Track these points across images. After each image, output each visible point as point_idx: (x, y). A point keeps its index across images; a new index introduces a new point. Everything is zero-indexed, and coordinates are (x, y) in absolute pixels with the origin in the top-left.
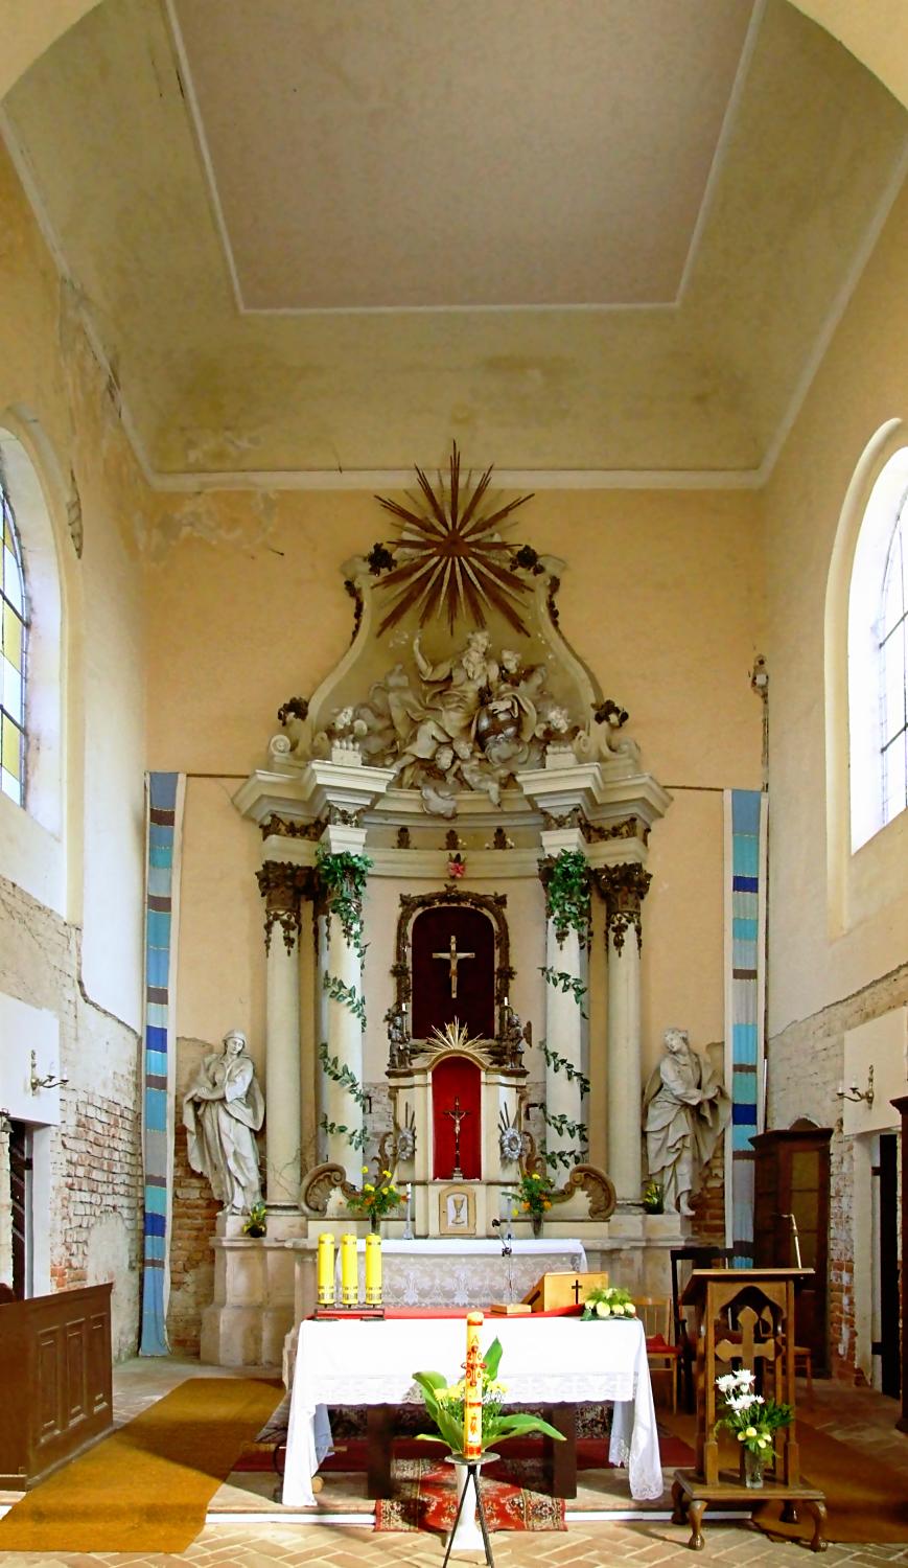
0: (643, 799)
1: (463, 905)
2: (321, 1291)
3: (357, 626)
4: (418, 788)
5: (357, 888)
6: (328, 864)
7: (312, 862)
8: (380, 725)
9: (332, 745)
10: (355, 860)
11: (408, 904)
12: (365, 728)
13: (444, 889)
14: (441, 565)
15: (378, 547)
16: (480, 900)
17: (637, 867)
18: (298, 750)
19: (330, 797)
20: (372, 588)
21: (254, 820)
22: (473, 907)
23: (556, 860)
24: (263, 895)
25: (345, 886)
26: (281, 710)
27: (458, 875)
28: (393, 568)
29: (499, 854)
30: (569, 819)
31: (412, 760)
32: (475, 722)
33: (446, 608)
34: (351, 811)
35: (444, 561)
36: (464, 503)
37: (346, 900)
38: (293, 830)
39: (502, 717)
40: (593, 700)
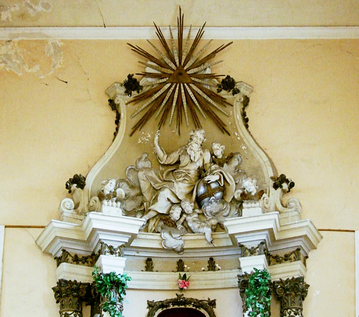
0: (306, 236)
1: (188, 306)
2: (225, 165)
3: (117, 129)
4: (158, 232)
5: (120, 296)
6: (102, 280)
7: (90, 280)
8: (133, 193)
9: (102, 204)
10: (119, 277)
11: (153, 307)
12: (124, 194)
13: (176, 297)
14: (172, 88)
15: (130, 77)
16: (199, 304)
17: (301, 280)
18: (80, 209)
19: (101, 237)
20: (127, 104)
21: (51, 255)
22: (194, 308)
23: (249, 275)
24: (57, 302)
25: (112, 293)
26: (67, 182)
27: (185, 288)
28: (140, 91)
29: (211, 274)
30: (258, 249)
31: (154, 214)
32: (195, 188)
33: (175, 117)
34: (115, 247)
35: (174, 86)
36: (186, 50)
37: (114, 303)
38: (76, 260)
39: (213, 186)
40: (271, 174)
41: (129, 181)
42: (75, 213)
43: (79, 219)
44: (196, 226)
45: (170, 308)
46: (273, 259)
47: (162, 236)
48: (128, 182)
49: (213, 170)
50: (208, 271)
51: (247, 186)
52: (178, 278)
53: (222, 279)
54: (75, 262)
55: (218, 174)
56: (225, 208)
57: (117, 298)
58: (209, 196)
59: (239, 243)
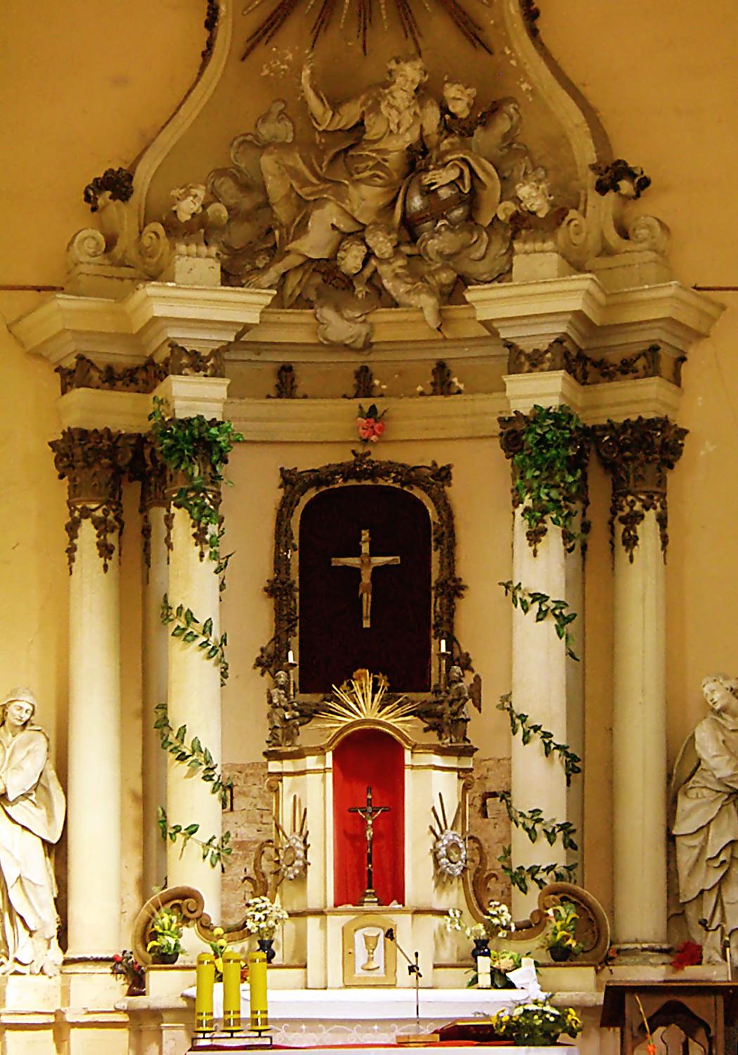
1: (381, 482)
3: (210, 45)
7: (144, 427)
16: (409, 475)
18: (117, 251)
19: (174, 333)
22: (397, 486)
26: (88, 187)
27: (374, 438)
29: (439, 403)
30: (549, 355)
31: (300, 260)
32: (401, 194)
41: (238, 175)
42: (107, 262)
43: (117, 278)
44: (403, 289)
45: (337, 486)
46: (592, 367)
47: (318, 316)
48: (234, 175)
49: (447, 152)
50: (432, 395)
51: (527, 197)
52: (357, 414)
53: (465, 416)
54: (107, 384)
55: (456, 165)
56: (476, 241)
57: (207, 475)
58: (433, 219)
59: (504, 339)
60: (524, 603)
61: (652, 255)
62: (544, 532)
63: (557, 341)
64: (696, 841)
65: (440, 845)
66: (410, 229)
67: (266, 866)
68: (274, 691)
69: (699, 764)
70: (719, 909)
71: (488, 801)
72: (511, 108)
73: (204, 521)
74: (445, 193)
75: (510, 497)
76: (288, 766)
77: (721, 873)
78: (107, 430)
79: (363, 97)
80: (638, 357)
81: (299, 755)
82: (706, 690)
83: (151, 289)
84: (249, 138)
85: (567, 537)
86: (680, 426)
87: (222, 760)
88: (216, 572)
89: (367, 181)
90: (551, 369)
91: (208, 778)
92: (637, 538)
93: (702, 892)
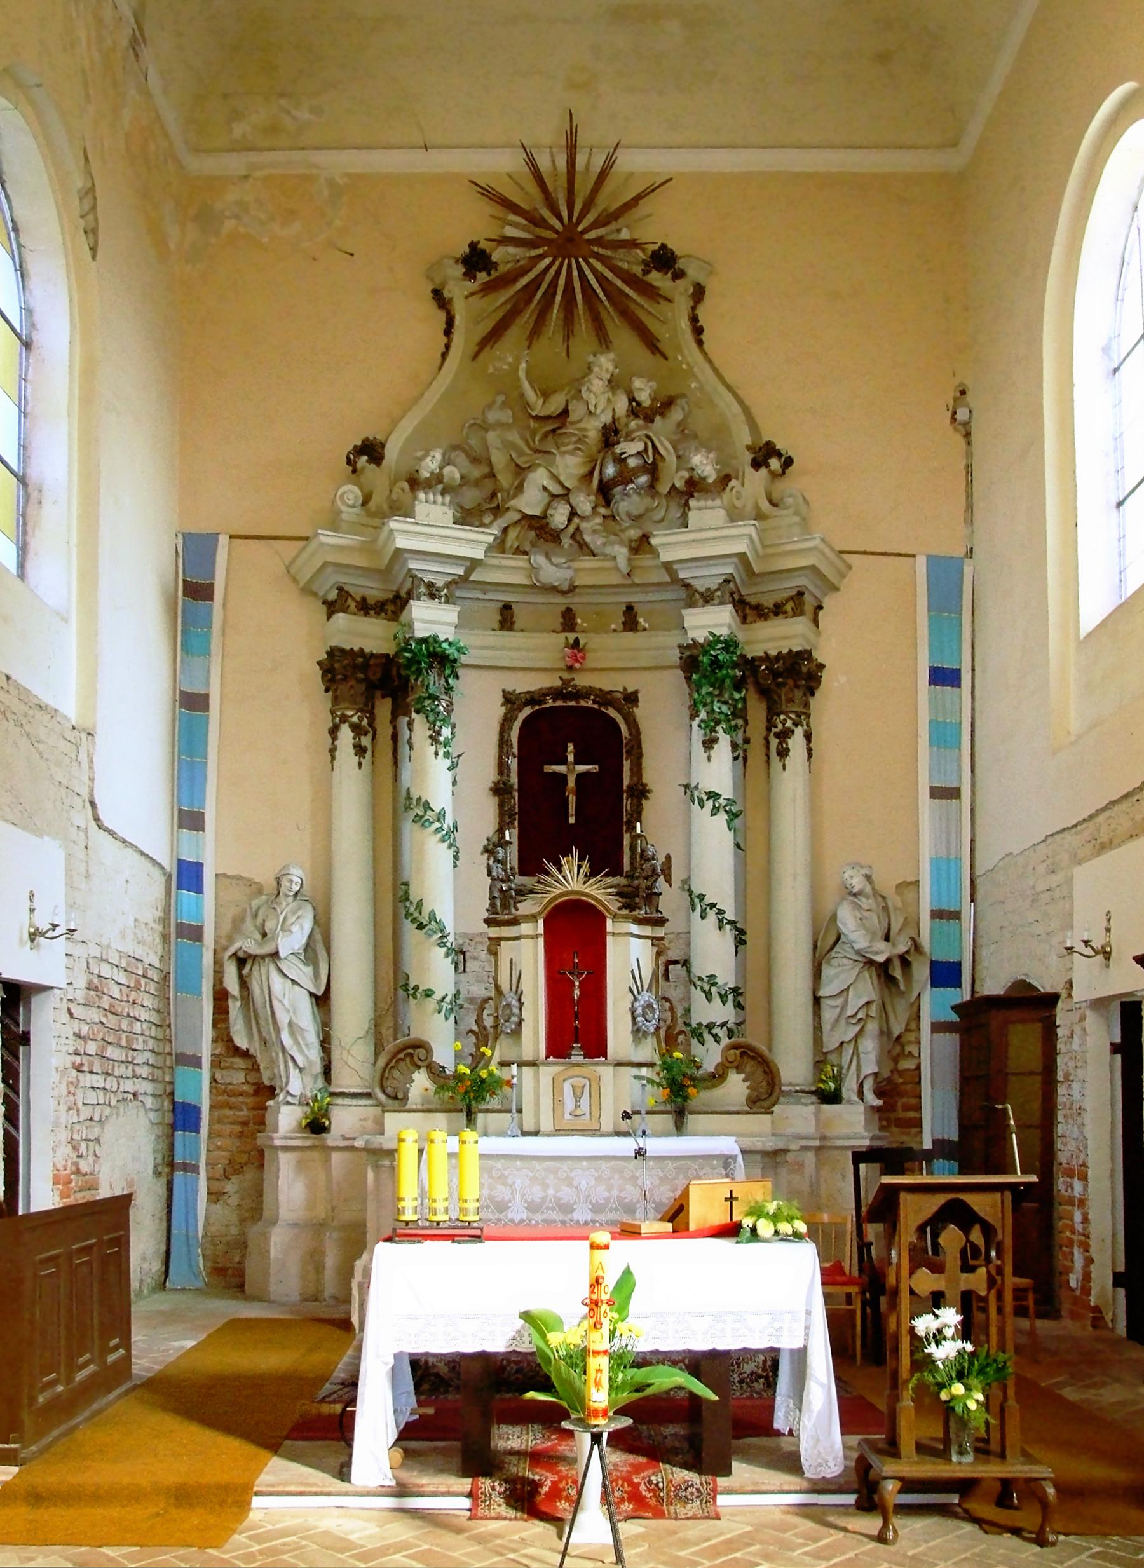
1: (583, 703)
7: (389, 648)
16: (605, 698)
18: (372, 505)
19: (413, 565)
22: (596, 706)
27: (577, 665)
30: (719, 593)
31: (517, 516)
60: (701, 801)
61: (796, 519)
62: (715, 741)
63: (725, 581)
64: (839, 1001)
65: (637, 1004)
66: (605, 492)
67: (488, 1022)
68: (494, 866)
69: (839, 938)
70: (855, 1058)
71: (670, 967)
72: (681, 402)
73: (438, 724)
74: (633, 462)
75: (686, 713)
76: (506, 932)
77: (857, 1028)
78: (361, 650)
79: (567, 389)
80: (787, 601)
81: (515, 922)
82: (846, 876)
83: (394, 524)
84: (478, 422)
85: (734, 746)
86: (820, 661)
87: (455, 928)
88: (449, 769)
89: (572, 453)
90: (721, 603)
91: (441, 944)
92: (788, 750)
93: (842, 1043)
